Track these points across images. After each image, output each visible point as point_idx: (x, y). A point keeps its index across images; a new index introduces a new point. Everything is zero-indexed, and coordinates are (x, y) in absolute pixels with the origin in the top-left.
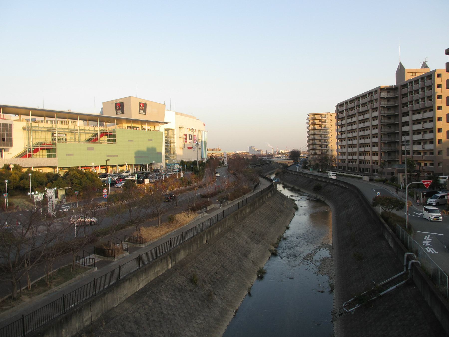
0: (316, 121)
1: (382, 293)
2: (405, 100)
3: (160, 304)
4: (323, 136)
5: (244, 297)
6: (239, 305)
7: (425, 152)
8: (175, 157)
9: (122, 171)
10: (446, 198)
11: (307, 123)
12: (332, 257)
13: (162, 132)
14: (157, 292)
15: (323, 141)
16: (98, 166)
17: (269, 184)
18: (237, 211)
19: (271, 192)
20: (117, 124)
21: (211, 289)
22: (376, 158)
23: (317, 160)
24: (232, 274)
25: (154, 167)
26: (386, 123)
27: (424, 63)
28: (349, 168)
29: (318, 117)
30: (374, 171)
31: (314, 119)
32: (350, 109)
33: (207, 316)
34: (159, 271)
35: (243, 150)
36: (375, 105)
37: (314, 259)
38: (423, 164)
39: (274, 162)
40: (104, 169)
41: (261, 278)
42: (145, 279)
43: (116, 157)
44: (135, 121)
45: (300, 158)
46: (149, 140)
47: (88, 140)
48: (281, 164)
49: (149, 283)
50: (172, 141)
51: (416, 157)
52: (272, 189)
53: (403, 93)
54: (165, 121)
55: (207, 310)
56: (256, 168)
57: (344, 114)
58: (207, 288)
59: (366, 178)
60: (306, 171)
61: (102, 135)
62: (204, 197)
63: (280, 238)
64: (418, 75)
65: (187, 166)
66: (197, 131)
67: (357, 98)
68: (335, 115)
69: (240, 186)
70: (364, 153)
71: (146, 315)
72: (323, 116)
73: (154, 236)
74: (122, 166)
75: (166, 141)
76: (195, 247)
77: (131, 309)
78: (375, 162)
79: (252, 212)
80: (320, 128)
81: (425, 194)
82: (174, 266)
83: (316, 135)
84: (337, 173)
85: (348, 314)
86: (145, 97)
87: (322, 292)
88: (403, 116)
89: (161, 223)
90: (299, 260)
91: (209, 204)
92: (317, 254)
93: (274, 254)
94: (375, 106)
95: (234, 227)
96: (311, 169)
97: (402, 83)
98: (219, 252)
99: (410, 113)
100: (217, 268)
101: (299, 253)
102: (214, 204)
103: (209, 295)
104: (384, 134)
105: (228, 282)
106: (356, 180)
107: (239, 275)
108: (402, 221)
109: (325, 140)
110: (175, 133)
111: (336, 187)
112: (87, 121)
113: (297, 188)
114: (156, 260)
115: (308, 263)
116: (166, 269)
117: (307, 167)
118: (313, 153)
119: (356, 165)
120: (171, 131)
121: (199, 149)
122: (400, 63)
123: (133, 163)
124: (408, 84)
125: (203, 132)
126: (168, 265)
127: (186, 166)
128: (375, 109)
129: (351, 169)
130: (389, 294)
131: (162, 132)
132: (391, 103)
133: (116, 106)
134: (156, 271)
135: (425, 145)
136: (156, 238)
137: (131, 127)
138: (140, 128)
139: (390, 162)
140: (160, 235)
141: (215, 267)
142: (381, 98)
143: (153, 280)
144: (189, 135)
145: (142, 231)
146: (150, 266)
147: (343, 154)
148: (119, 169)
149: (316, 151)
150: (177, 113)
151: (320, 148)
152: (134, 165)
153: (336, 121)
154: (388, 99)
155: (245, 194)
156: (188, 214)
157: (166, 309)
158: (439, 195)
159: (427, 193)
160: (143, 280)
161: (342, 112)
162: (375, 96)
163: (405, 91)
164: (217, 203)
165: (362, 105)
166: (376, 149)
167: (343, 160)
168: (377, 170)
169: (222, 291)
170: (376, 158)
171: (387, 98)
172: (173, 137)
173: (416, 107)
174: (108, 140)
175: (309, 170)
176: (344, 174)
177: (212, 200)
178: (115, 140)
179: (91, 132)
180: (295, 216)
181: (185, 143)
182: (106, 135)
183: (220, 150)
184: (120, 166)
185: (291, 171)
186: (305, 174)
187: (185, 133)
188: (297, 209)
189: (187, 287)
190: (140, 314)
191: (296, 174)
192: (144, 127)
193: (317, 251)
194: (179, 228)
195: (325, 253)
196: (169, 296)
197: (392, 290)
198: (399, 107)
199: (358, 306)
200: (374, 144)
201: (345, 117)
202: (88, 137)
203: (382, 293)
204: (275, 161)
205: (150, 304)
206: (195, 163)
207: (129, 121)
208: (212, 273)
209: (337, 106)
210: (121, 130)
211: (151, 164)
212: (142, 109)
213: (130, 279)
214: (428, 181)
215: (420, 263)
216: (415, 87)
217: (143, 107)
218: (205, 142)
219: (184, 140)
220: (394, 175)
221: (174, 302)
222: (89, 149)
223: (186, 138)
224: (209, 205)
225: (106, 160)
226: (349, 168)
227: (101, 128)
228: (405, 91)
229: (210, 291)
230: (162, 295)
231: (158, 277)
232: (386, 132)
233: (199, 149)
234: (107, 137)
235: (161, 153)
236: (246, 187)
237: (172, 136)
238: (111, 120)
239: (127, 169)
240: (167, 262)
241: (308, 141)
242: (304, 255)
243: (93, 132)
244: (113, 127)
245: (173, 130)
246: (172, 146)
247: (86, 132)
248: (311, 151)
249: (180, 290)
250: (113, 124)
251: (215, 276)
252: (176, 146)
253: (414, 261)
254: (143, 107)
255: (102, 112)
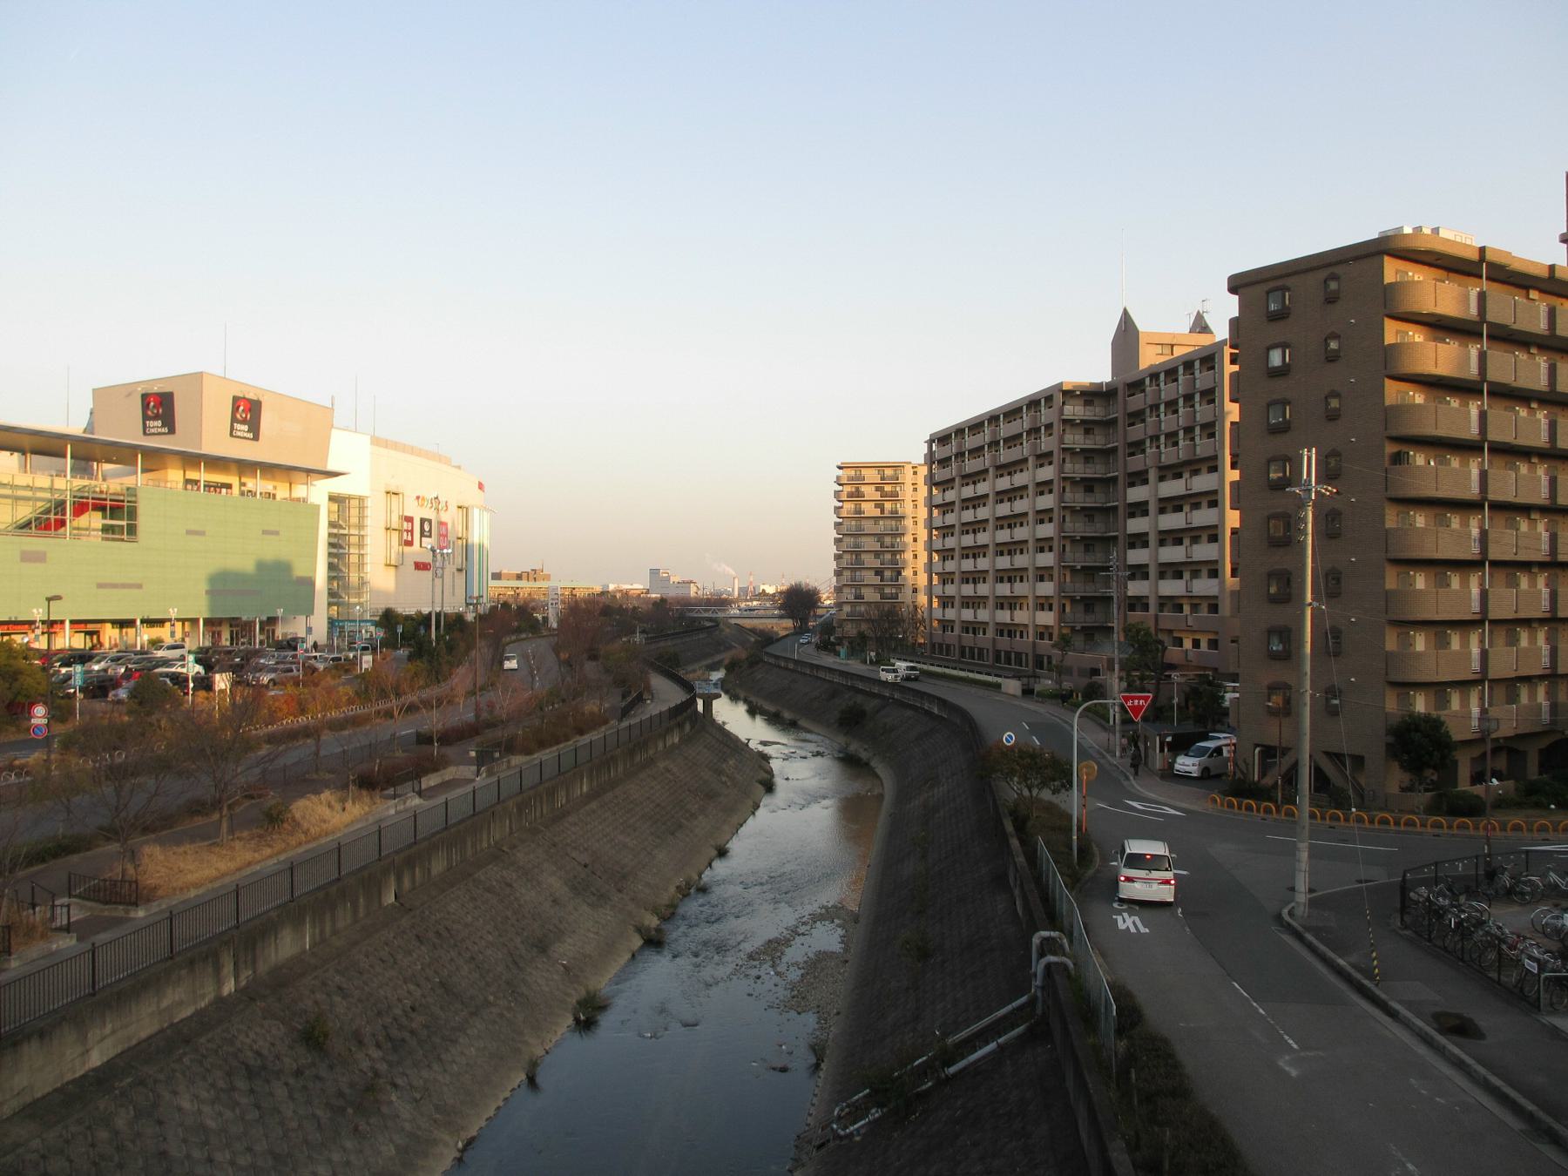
0: (863, 488)
1: (952, 1070)
2: (1137, 432)
3: (160, 1123)
4: (888, 540)
5: (507, 1094)
6: (483, 1123)
7: (1196, 602)
8: (365, 598)
9: (156, 643)
10: (1225, 754)
11: (837, 494)
12: (846, 950)
13: (317, 508)
14: (156, 1081)
15: (888, 557)
16: (62, 622)
17: (675, 696)
18: (532, 792)
19: (680, 726)
20: (144, 471)
21: (382, 1067)
22: (1047, 618)
23: (867, 621)
24: (473, 1014)
25: (280, 632)
26: (1078, 505)
27: (1199, 317)
28: (997, 654)
29: (871, 476)
30: (1039, 662)
31: (857, 481)
32: (970, 452)
33: (348, 1163)
34: (181, 1003)
35: (628, 579)
36: (1046, 443)
37: (785, 959)
38: (1188, 644)
39: (729, 626)
40: (87, 633)
41: (586, 1024)
42: (113, 1032)
43: (136, 591)
44: (216, 463)
45: (819, 611)
46: (265, 532)
47: (27, 525)
48: (753, 631)
49: (129, 1049)
50: (354, 540)
51: (1168, 618)
52: (691, 720)
53: (1132, 408)
54: (330, 467)
55: (349, 1144)
56: (662, 644)
57: (952, 471)
58: (365, 1065)
59: (1012, 686)
60: (828, 660)
61: (80, 509)
62: (424, 739)
63: (689, 886)
64: (1178, 352)
65: (401, 630)
66: (453, 508)
67: (993, 418)
68: (924, 471)
69: (567, 708)
70: (1011, 603)
71: (95, 1164)
72: (889, 472)
73: (190, 878)
74: (160, 622)
75: (334, 540)
76: (344, 918)
77: (36, 1143)
78: (1043, 632)
79: (594, 795)
80: (877, 512)
81: (1169, 739)
82: (246, 988)
83: (865, 540)
84: (925, 667)
85: (845, 1142)
86: (253, 378)
87: (784, 1070)
88: (1132, 485)
89: (231, 831)
90: (732, 960)
91: (435, 766)
92: (799, 940)
93: (654, 942)
94: (1044, 448)
95: (513, 847)
96: (843, 651)
97: (1131, 377)
98: (438, 933)
99: (1152, 475)
100: (418, 993)
101: (741, 938)
102: (458, 764)
103: (370, 1089)
104: (1073, 540)
105: (454, 1042)
106: (981, 692)
107: (501, 1015)
108: (1060, 822)
109: (894, 553)
110: (368, 512)
111: (909, 713)
112: (24, 453)
113: (787, 715)
114: (170, 963)
115: (762, 973)
116: (210, 997)
117: (833, 644)
118: (851, 598)
119: (985, 639)
120: (354, 503)
121: (460, 570)
122: (1125, 312)
123: (201, 610)
124: (1147, 381)
125: (476, 511)
126: (219, 983)
127: (400, 630)
128: (1044, 458)
129: (970, 656)
130: (974, 1069)
131: (317, 508)
132: (1097, 441)
133: (145, 406)
134: (165, 1003)
135: (1195, 581)
136: (196, 885)
137: (196, 482)
138: (236, 490)
139: (1090, 633)
140: (215, 873)
141: (412, 987)
142: (1065, 421)
143: (150, 1037)
144: (422, 521)
145: (146, 860)
146: (142, 984)
147: (946, 602)
148: (145, 635)
149: (864, 591)
150: (376, 441)
151: (877, 580)
152: (207, 622)
153: (923, 491)
154: (1088, 427)
155: (581, 732)
156: (343, 801)
157: (185, 1141)
158: (1211, 744)
159: (1174, 736)
160: (103, 1039)
161: (944, 462)
162: (1046, 415)
163: (1137, 402)
164: (469, 762)
165: (1005, 440)
166: (1047, 588)
167: (946, 625)
168: (1049, 657)
169: (425, 1073)
170: (1047, 618)
171: (1083, 422)
172: (361, 526)
173: (1169, 455)
174: (106, 529)
175: (837, 654)
176: (947, 671)
177: (450, 751)
178: (132, 530)
179: (39, 495)
180: (759, 813)
181: (407, 549)
182: (96, 508)
183: (547, 578)
184: (150, 622)
185: (777, 657)
186: (818, 667)
187: (407, 514)
188: (769, 787)
189: (287, 1060)
190: (71, 1161)
191: (791, 666)
192: (251, 484)
193: (802, 929)
194: (301, 850)
195: (828, 938)
196: (204, 1094)
197: (984, 1057)
198: (1120, 452)
199: (875, 1113)
200: (1043, 574)
201: (953, 480)
202: (25, 512)
203: (952, 1070)
204: (733, 621)
205: (121, 1122)
206: (425, 620)
207: (191, 460)
208: (398, 1011)
209: (930, 442)
210: (162, 496)
211: (272, 621)
212: (244, 422)
213: (42, 1034)
214: (1139, 698)
215: (1071, 965)
216: (1167, 391)
217: (248, 412)
218: (481, 547)
219: (401, 537)
220: (1095, 678)
221: (220, 1114)
222: (27, 557)
223: (406, 530)
224: (435, 770)
225: (49, 600)
226: (997, 654)
227: (79, 482)
228: (1137, 402)
229: (377, 1074)
230: (175, 1093)
231: (172, 1025)
232: (1078, 536)
233: (460, 570)
234: (104, 517)
235: (310, 583)
236: (591, 706)
237: (354, 520)
238: (122, 454)
239: (173, 634)
240: (218, 969)
241: (838, 557)
242: (756, 943)
243: (48, 495)
244: (129, 481)
245: (361, 499)
246: (354, 559)
247: (21, 493)
248: (846, 590)
249: (251, 1073)
250: (128, 468)
251: (404, 1021)
252: (368, 559)
253: (1052, 959)
254: (248, 412)
255: (90, 427)
